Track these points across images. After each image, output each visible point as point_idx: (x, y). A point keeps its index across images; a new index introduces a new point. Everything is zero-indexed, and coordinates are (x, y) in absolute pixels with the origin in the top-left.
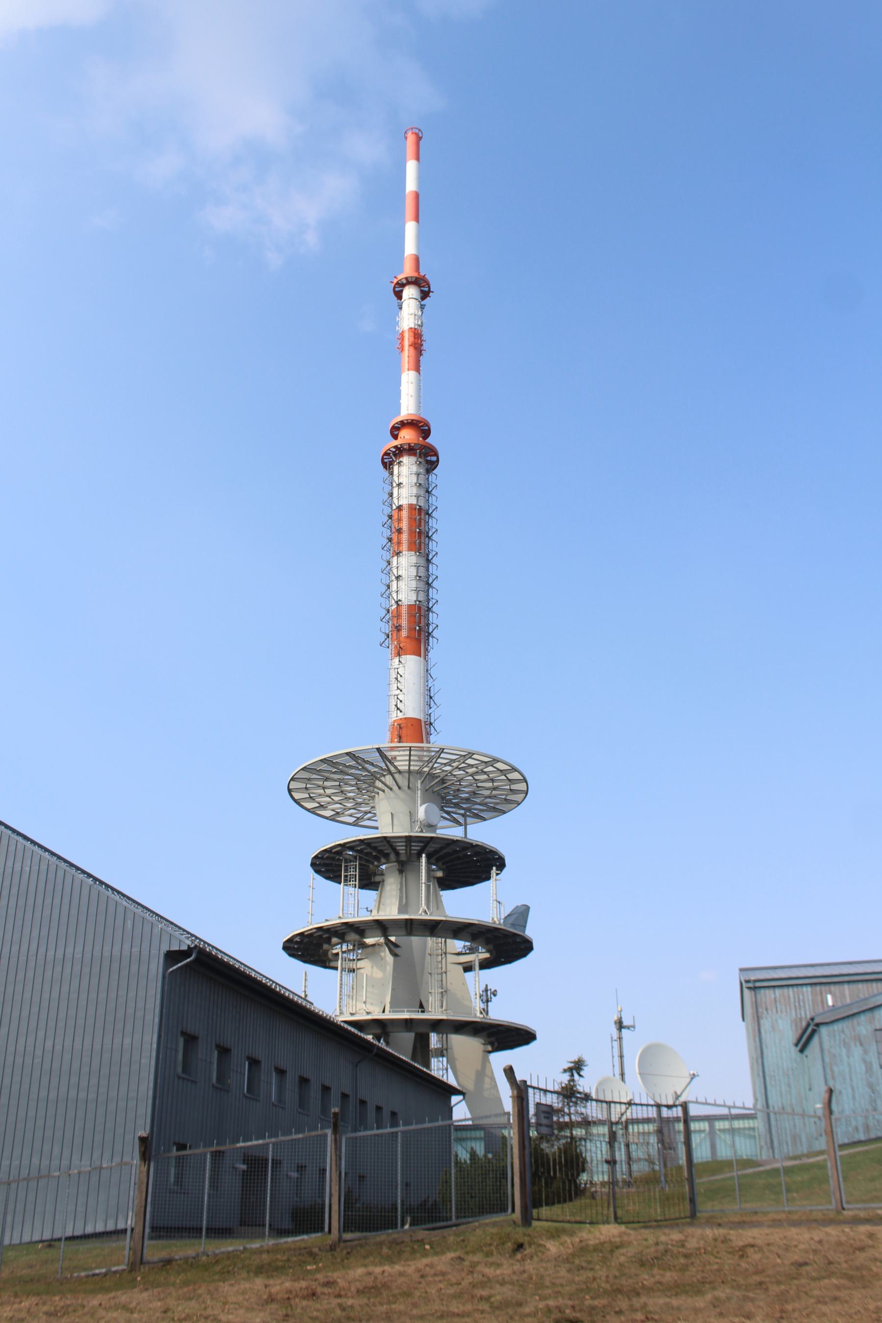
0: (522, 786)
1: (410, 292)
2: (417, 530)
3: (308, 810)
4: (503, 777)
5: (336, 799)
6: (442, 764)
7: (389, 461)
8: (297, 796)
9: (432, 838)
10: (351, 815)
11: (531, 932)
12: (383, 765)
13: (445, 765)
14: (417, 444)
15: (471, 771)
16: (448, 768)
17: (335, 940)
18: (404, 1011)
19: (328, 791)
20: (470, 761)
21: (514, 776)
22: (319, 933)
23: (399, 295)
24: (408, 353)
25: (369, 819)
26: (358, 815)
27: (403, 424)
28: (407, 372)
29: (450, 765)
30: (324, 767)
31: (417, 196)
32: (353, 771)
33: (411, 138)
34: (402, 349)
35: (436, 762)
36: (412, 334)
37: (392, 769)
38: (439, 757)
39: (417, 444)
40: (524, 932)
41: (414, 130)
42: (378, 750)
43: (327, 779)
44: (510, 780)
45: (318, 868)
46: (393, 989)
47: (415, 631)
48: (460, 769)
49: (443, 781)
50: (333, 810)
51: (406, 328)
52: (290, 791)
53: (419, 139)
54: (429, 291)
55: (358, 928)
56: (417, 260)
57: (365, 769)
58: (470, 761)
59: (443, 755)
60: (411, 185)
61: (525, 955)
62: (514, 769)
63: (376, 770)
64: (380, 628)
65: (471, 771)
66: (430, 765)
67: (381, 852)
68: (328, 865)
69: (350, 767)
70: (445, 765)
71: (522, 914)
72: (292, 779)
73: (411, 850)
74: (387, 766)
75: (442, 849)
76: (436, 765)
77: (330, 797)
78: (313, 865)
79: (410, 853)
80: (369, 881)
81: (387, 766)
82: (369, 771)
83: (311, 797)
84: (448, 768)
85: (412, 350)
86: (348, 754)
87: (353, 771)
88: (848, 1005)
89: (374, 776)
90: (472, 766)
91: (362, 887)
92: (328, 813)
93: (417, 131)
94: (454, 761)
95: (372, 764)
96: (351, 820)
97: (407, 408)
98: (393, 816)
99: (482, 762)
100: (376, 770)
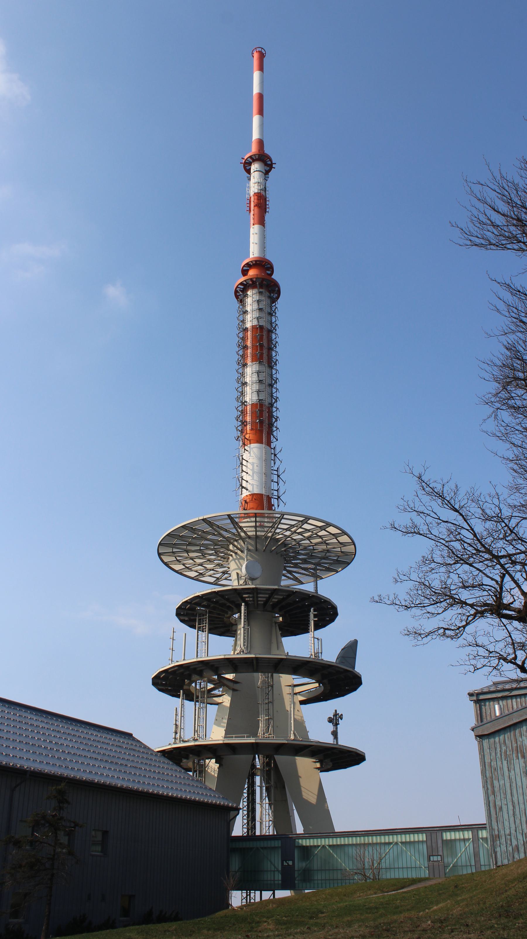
0: (351, 548)
1: (255, 167)
2: (263, 345)
3: (176, 572)
4: (335, 541)
5: (198, 561)
6: (284, 529)
7: (240, 294)
8: (166, 559)
9: (275, 590)
10: (210, 576)
11: (359, 668)
12: (234, 531)
13: (287, 530)
14: (263, 279)
15: (306, 535)
16: (288, 533)
17: (194, 677)
18: (232, 737)
19: (192, 555)
20: (306, 526)
21: (344, 539)
22: (181, 671)
23: (248, 171)
24: (254, 210)
25: (226, 579)
26: (218, 576)
27: (249, 266)
28: (252, 226)
29: (290, 530)
30: (185, 533)
31: (261, 97)
32: (209, 537)
33: (256, 55)
34: (250, 210)
35: (277, 528)
36: (256, 197)
37: (243, 534)
38: (280, 523)
39: (263, 279)
40: (354, 668)
41: (258, 50)
42: (229, 516)
43: (190, 544)
44: (341, 543)
45: (182, 618)
46: (229, 719)
47: (262, 423)
48: (299, 534)
49: (284, 544)
50: (196, 571)
51: (252, 194)
52: (160, 554)
53: (262, 56)
54: (272, 164)
55: (213, 666)
56: (261, 143)
57: (220, 535)
58: (306, 526)
59: (283, 521)
60: (256, 90)
61: (355, 690)
62: (344, 533)
63: (229, 535)
64: (232, 425)
65: (306, 535)
66: (273, 530)
67: (232, 602)
68: (188, 613)
69: (208, 533)
70: (287, 530)
71: (350, 651)
72: (160, 544)
73: (258, 601)
74: (238, 532)
75: (283, 599)
76: (278, 531)
77: (213, 570)
78: (178, 614)
79: (258, 604)
80: (225, 629)
81: (238, 532)
82: (224, 537)
83: (178, 560)
84: (288, 533)
85: (256, 209)
86: (204, 520)
87: (209, 537)
88: (497, 718)
89: (229, 541)
90: (309, 531)
91: (213, 630)
92: (193, 574)
93: (260, 49)
94: (293, 526)
95: (226, 531)
96: (212, 580)
97: (254, 252)
98: (237, 572)
99: (317, 526)
100: (229, 535)
